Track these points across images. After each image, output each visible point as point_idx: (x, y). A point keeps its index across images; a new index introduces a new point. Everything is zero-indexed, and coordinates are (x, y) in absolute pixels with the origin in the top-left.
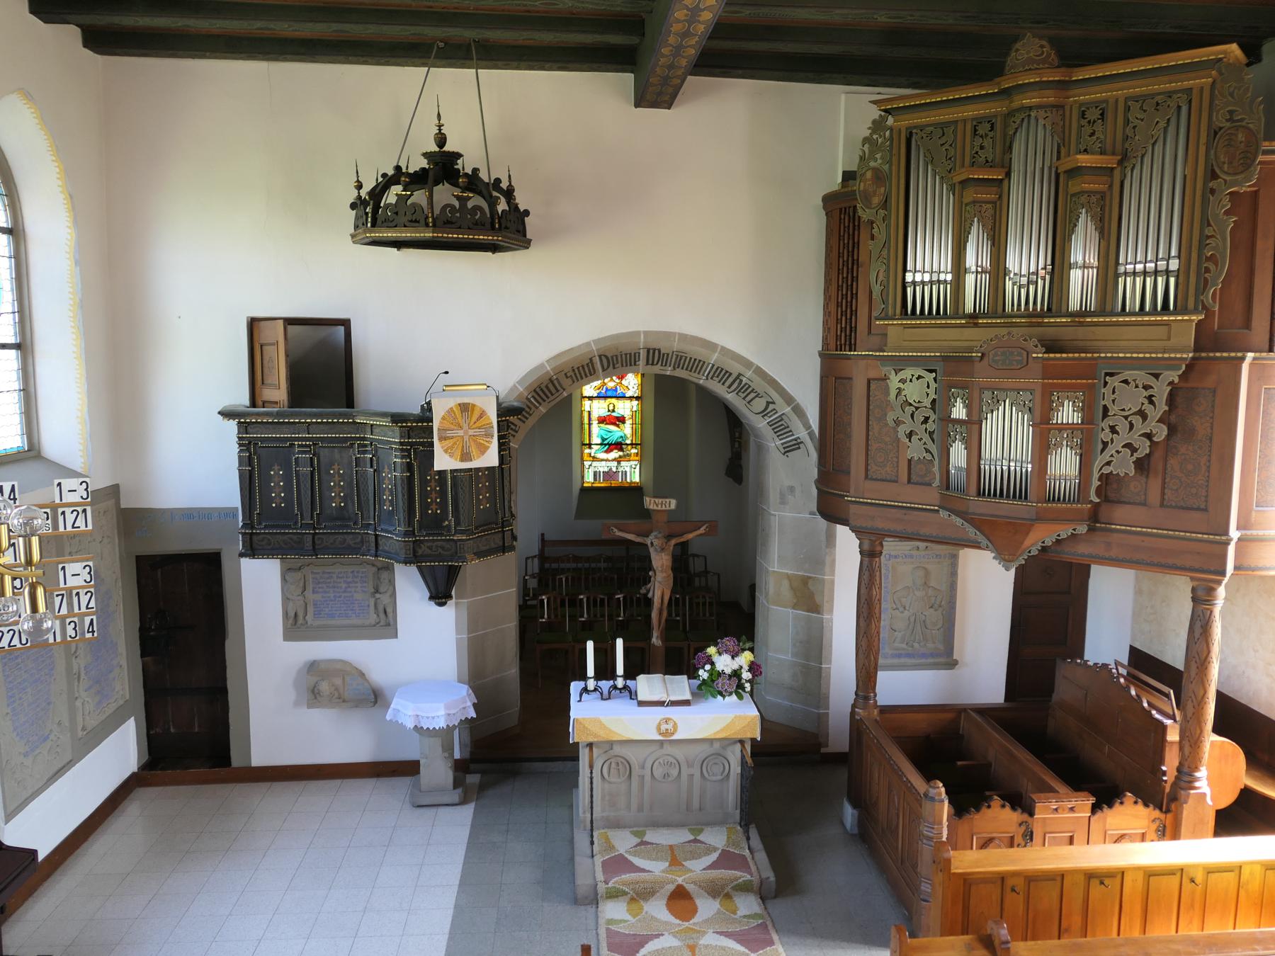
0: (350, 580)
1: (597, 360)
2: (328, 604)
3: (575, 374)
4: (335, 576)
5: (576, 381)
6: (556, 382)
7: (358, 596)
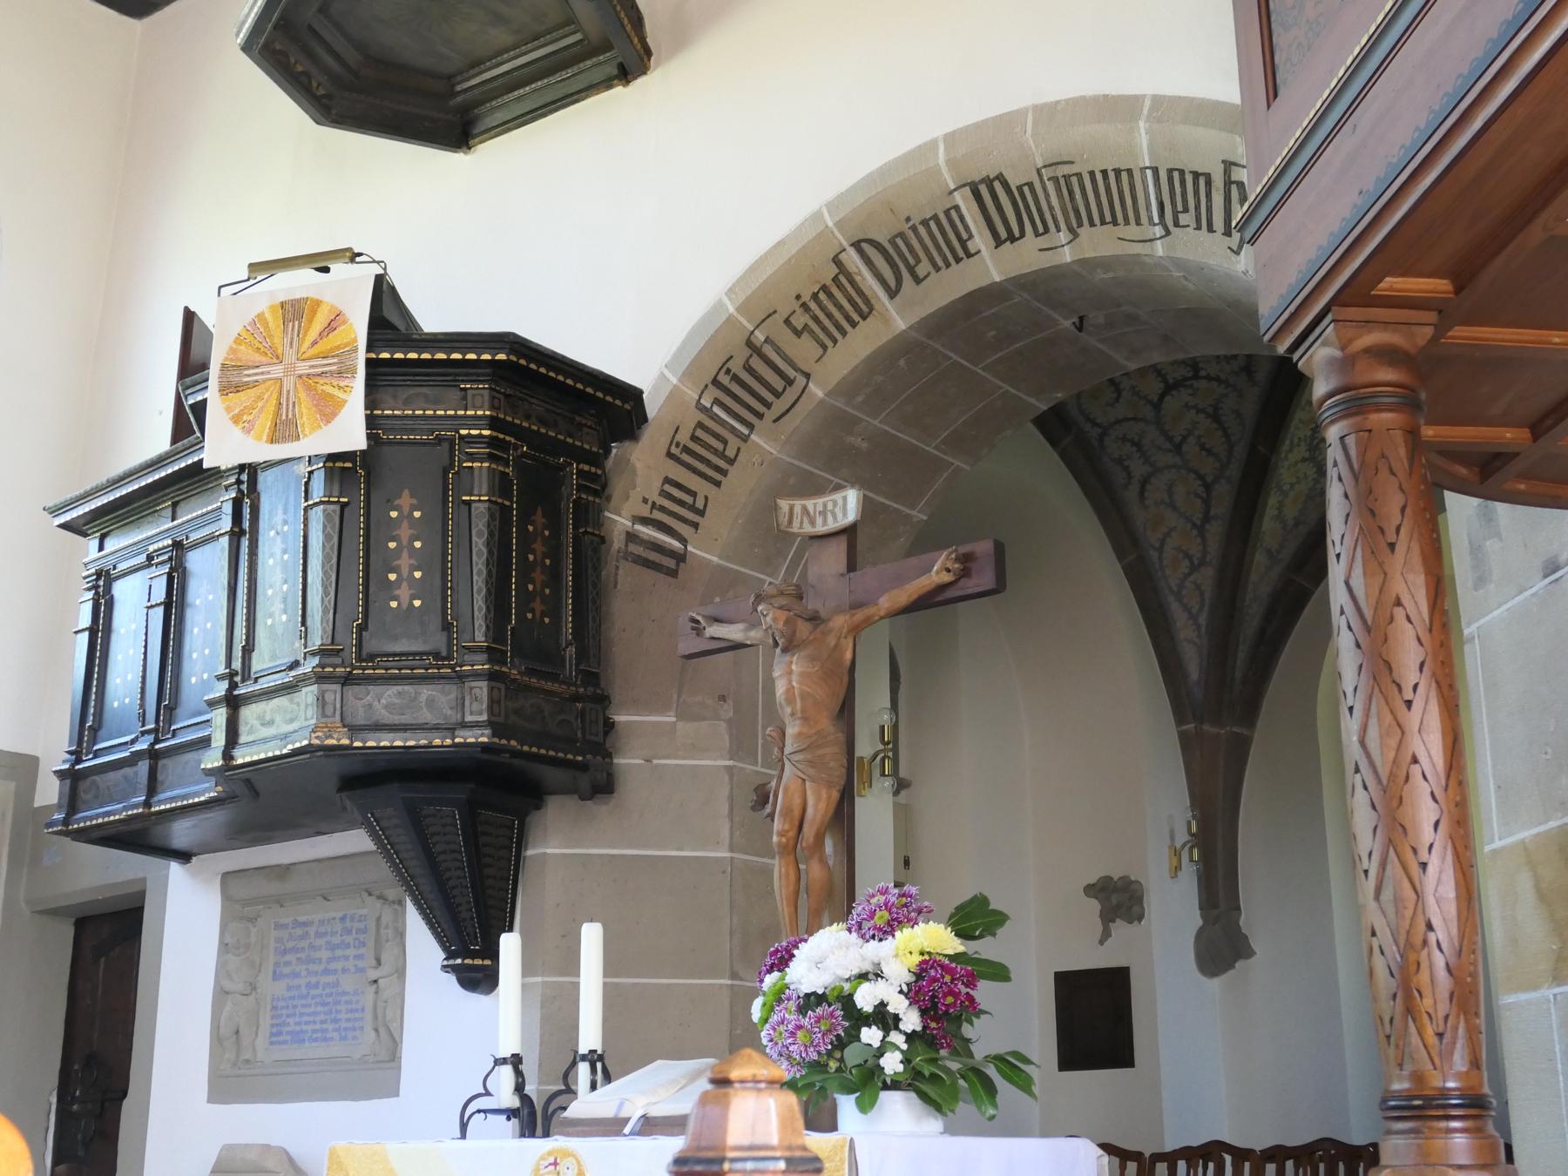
0: (336, 940)
1: (852, 259)
2: (295, 1007)
3: (816, 319)
4: (312, 931)
5: (829, 343)
6: (769, 351)
7: (348, 983)
